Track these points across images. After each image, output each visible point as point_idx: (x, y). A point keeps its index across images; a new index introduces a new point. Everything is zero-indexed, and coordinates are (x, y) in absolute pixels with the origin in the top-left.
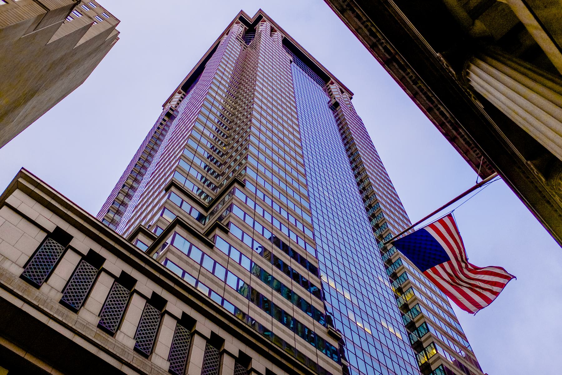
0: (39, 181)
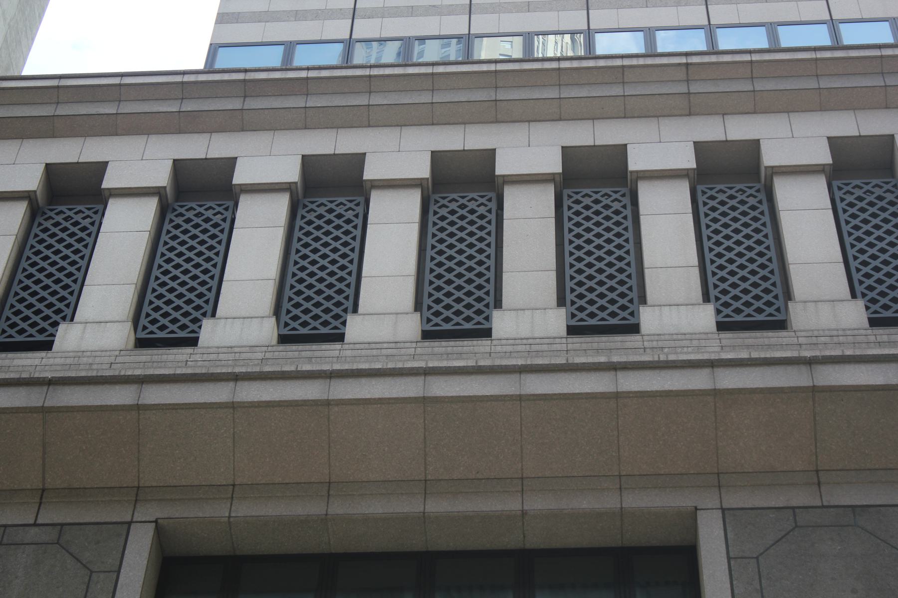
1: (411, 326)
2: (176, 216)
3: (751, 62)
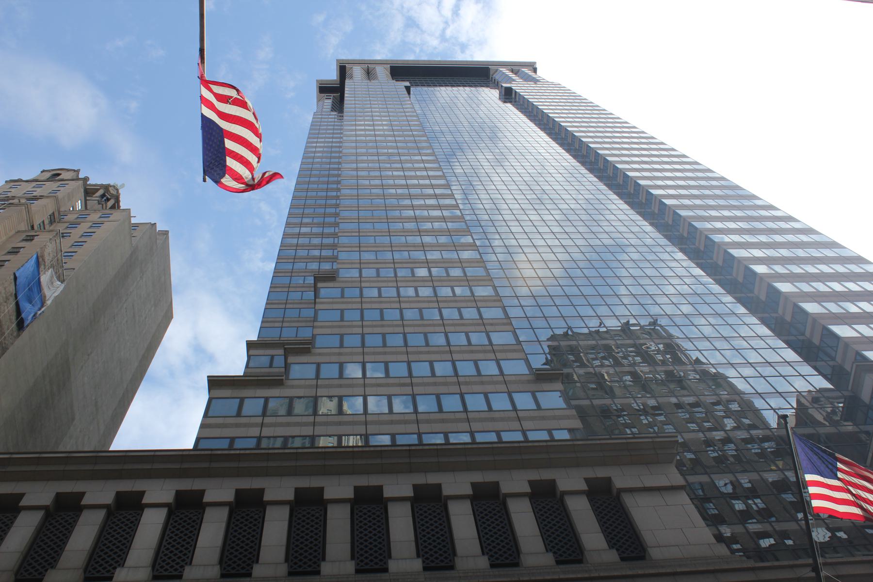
0: (209, 452)
1: (283, 570)
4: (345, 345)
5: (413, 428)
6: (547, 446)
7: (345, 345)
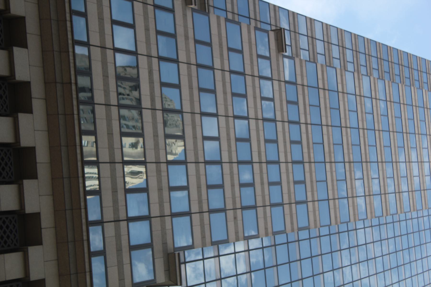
2: (5, 153)
3: (73, 114)
4: (211, 191)
5: (109, 215)
6: (83, 240)
7: (210, 191)
